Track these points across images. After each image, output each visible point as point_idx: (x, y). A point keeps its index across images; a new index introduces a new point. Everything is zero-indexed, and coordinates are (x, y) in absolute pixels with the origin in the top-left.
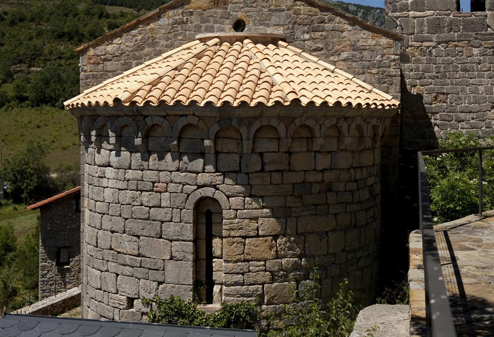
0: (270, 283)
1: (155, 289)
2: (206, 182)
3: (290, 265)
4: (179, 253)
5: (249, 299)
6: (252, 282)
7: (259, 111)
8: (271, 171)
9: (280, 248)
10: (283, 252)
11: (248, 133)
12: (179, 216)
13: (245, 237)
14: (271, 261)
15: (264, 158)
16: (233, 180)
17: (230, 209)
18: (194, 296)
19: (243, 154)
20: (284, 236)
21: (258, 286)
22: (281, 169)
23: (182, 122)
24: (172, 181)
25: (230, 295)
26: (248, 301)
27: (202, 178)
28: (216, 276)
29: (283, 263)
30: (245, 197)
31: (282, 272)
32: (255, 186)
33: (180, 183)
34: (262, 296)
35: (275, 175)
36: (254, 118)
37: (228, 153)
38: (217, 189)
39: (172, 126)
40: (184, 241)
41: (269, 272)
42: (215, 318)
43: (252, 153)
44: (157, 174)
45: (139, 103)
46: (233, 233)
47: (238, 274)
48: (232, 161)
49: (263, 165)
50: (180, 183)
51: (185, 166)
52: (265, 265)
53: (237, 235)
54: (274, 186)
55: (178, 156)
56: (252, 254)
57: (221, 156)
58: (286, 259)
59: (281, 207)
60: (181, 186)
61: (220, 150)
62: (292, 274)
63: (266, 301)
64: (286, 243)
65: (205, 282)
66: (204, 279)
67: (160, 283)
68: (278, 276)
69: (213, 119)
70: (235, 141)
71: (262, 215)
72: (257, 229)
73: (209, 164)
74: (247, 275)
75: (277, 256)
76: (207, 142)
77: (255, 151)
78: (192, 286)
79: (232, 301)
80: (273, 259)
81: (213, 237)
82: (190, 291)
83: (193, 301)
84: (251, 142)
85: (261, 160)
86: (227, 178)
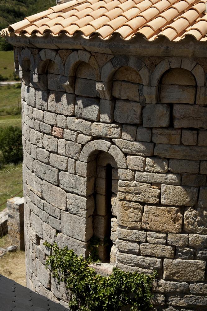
0: (171, 259)
1: (53, 236)
2: (101, 134)
3: (199, 243)
4: (74, 206)
5: (144, 270)
6: (149, 254)
7: (163, 48)
8: (182, 129)
9: (188, 222)
10: (190, 227)
11: (150, 77)
12: (74, 167)
13: (143, 204)
14: (174, 234)
15: (174, 111)
16: (131, 135)
17: (127, 168)
18: (87, 254)
19: (146, 104)
20: (195, 208)
21: (156, 259)
22: (196, 127)
23: (73, 59)
24: (67, 127)
25: (124, 262)
26: (142, 273)
27: (98, 129)
28: (114, 237)
29: (190, 239)
30: (146, 157)
31: (188, 249)
32: (160, 146)
33: (75, 131)
34: (160, 271)
35: (186, 134)
36: (159, 57)
37: (127, 100)
38: (113, 143)
39: (64, 63)
40: (78, 195)
41: (171, 245)
42: (105, 282)
43: (157, 103)
44: (55, 117)
45: (85, 35)
46: (129, 197)
47: (133, 242)
48: (131, 111)
49: (172, 119)
50: (75, 131)
51: (80, 111)
52: (166, 238)
53: (133, 200)
54: (184, 148)
55: (73, 101)
56: (151, 223)
57: (119, 104)
58: (195, 235)
59: (193, 174)
60: (76, 134)
61: (117, 96)
62: (200, 252)
63: (164, 276)
64: (196, 216)
65: (102, 240)
66: (102, 237)
67: (58, 231)
68: (182, 253)
69: (106, 56)
70: (136, 86)
71: (167, 181)
72: (159, 197)
73: (104, 113)
74: (144, 245)
75: (183, 230)
76: (99, 86)
77: (162, 102)
78: (85, 243)
79: (126, 269)
80: (177, 233)
81: (113, 195)
82: (83, 247)
83: (87, 257)
84: (154, 90)
85: (168, 113)
86: (124, 131)
